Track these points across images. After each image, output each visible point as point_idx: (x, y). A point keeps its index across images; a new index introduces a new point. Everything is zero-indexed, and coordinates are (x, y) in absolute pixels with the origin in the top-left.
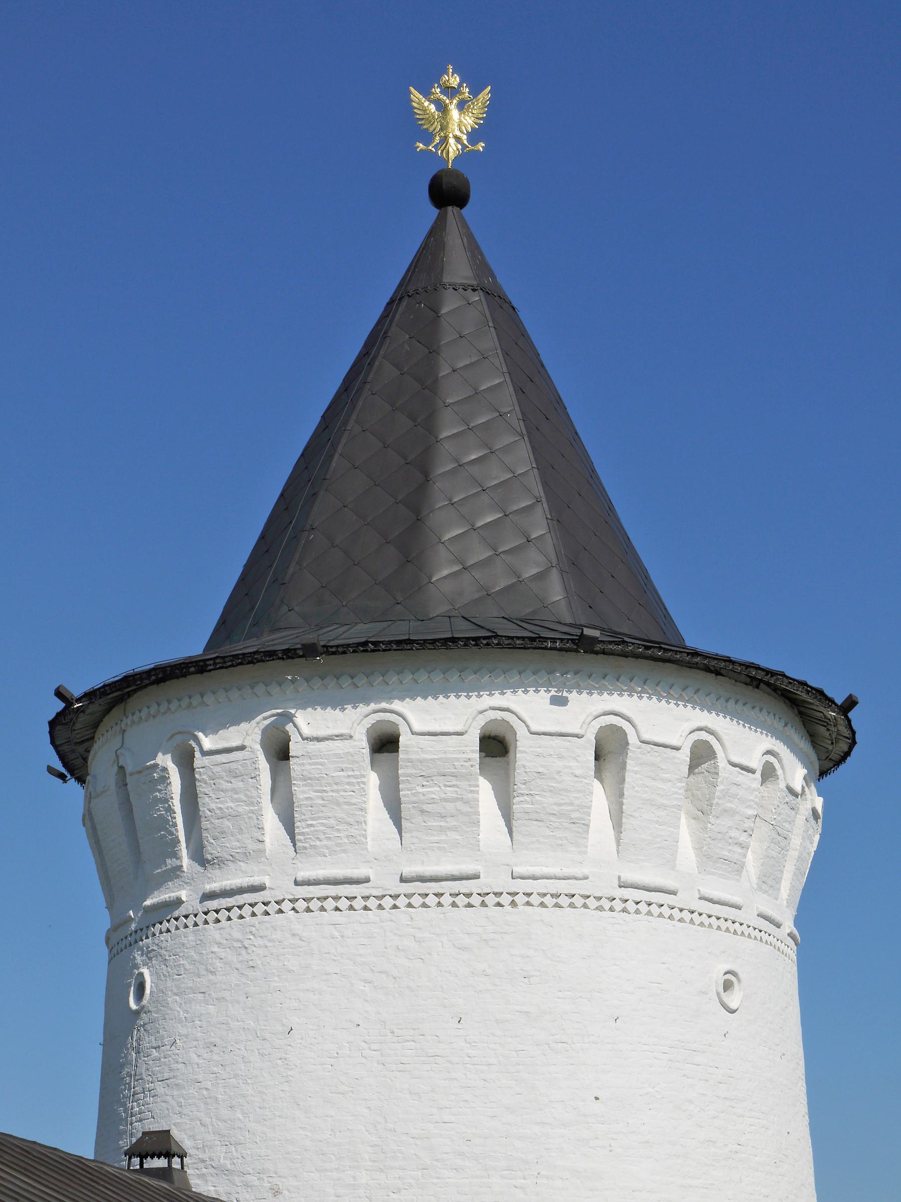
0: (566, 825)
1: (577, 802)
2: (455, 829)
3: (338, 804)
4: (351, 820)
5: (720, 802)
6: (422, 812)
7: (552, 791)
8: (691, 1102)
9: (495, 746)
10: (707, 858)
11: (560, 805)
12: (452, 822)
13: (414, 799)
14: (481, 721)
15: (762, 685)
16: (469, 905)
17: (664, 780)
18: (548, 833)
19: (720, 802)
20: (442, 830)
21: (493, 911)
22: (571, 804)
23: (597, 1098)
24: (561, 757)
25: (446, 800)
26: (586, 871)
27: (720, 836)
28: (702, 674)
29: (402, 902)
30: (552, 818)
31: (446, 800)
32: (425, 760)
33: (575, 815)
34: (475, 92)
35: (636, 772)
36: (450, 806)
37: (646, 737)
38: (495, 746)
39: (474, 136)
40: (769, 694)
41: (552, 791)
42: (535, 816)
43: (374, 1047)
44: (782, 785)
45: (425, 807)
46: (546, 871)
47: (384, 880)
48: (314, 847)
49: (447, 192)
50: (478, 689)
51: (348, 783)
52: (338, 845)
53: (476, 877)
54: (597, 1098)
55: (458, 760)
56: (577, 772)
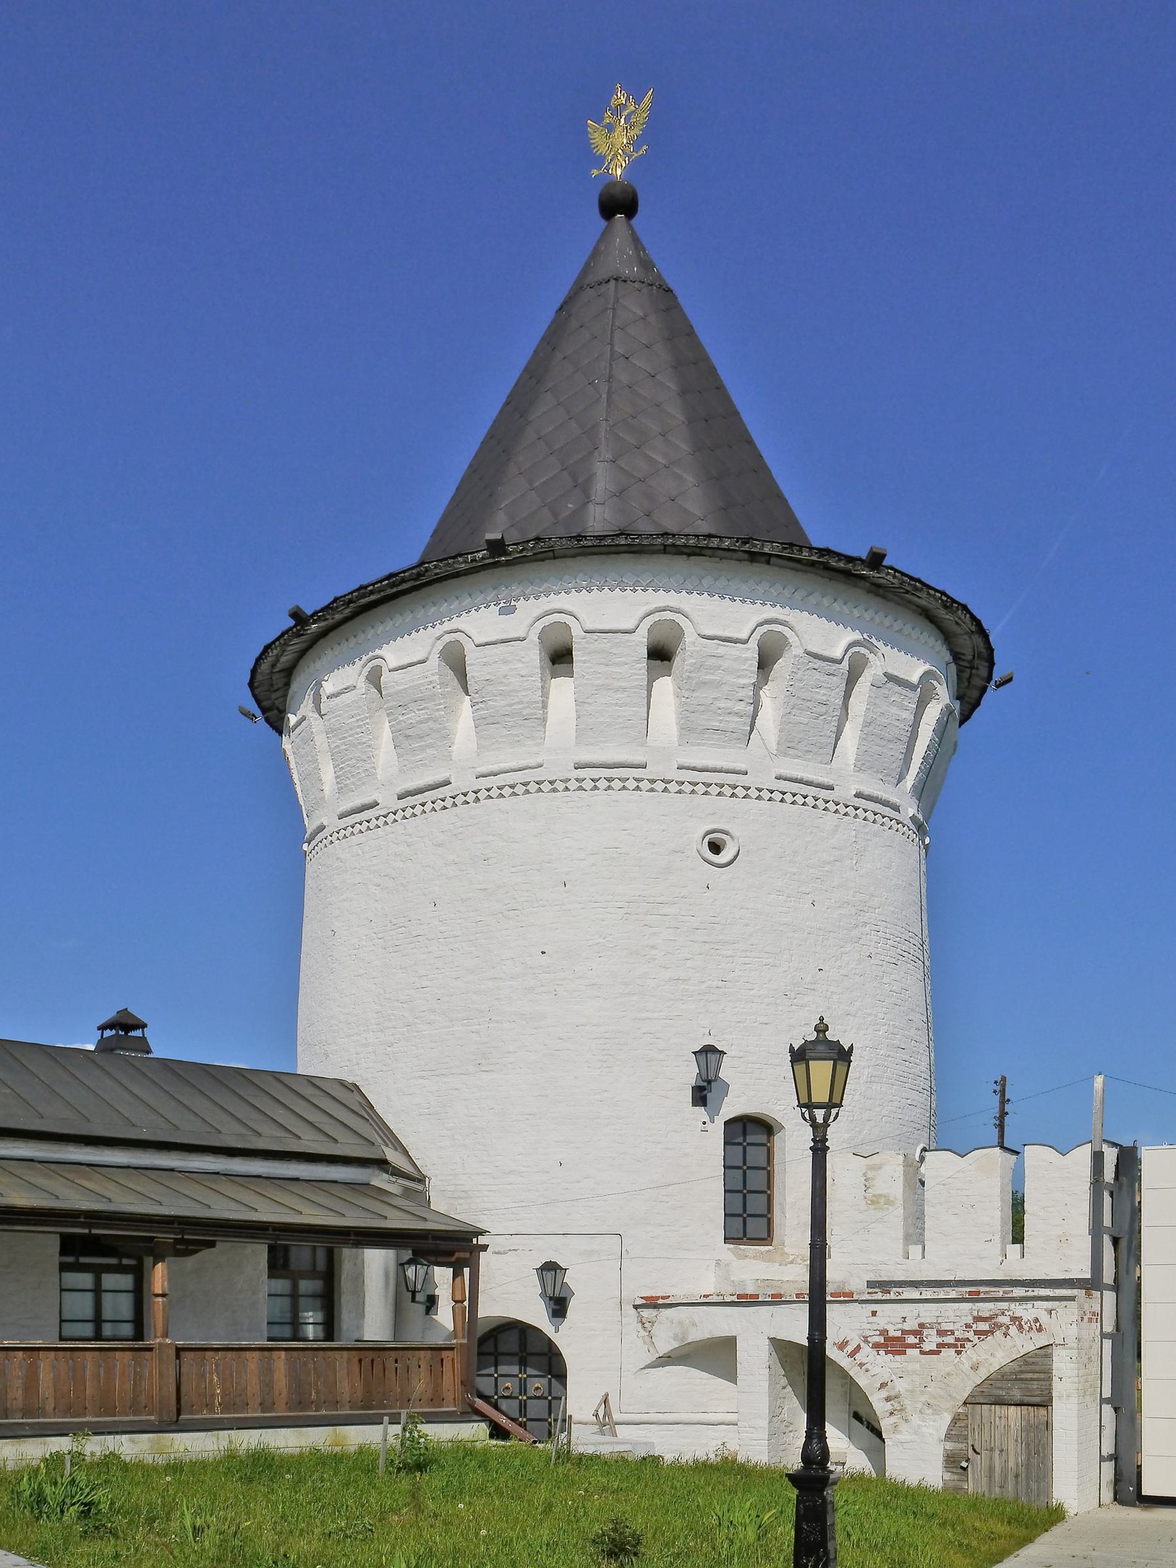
0: (521, 722)
1: (526, 700)
2: (431, 746)
3: (355, 746)
4: (364, 757)
5: (693, 675)
6: (407, 736)
7: (502, 694)
8: (653, 947)
9: (456, 662)
10: (688, 730)
11: (511, 705)
12: (430, 741)
13: (399, 727)
14: (440, 645)
15: (773, 560)
16: (445, 808)
17: (618, 664)
18: (505, 732)
19: (693, 675)
20: (423, 749)
21: (462, 808)
22: (521, 702)
23: (543, 953)
24: (506, 662)
25: (421, 722)
26: (539, 760)
27: (702, 708)
28: (665, 559)
29: (673, 787)
30: (507, 719)
31: (421, 722)
32: (400, 691)
33: (525, 712)
34: (638, 102)
35: (584, 662)
36: (424, 726)
37: (589, 626)
38: (456, 662)
39: (636, 143)
40: (806, 572)
41: (502, 694)
42: (490, 720)
43: (380, 936)
44: (800, 652)
45: (408, 732)
46: (503, 766)
47: (387, 801)
48: (346, 785)
49: (618, 204)
50: (440, 618)
51: (358, 727)
52: (360, 779)
53: (447, 783)
54: (543, 953)
55: (422, 684)
56: (523, 673)
